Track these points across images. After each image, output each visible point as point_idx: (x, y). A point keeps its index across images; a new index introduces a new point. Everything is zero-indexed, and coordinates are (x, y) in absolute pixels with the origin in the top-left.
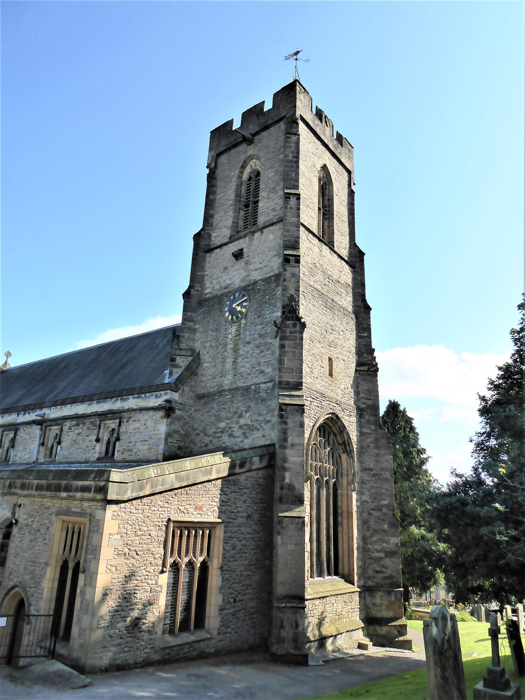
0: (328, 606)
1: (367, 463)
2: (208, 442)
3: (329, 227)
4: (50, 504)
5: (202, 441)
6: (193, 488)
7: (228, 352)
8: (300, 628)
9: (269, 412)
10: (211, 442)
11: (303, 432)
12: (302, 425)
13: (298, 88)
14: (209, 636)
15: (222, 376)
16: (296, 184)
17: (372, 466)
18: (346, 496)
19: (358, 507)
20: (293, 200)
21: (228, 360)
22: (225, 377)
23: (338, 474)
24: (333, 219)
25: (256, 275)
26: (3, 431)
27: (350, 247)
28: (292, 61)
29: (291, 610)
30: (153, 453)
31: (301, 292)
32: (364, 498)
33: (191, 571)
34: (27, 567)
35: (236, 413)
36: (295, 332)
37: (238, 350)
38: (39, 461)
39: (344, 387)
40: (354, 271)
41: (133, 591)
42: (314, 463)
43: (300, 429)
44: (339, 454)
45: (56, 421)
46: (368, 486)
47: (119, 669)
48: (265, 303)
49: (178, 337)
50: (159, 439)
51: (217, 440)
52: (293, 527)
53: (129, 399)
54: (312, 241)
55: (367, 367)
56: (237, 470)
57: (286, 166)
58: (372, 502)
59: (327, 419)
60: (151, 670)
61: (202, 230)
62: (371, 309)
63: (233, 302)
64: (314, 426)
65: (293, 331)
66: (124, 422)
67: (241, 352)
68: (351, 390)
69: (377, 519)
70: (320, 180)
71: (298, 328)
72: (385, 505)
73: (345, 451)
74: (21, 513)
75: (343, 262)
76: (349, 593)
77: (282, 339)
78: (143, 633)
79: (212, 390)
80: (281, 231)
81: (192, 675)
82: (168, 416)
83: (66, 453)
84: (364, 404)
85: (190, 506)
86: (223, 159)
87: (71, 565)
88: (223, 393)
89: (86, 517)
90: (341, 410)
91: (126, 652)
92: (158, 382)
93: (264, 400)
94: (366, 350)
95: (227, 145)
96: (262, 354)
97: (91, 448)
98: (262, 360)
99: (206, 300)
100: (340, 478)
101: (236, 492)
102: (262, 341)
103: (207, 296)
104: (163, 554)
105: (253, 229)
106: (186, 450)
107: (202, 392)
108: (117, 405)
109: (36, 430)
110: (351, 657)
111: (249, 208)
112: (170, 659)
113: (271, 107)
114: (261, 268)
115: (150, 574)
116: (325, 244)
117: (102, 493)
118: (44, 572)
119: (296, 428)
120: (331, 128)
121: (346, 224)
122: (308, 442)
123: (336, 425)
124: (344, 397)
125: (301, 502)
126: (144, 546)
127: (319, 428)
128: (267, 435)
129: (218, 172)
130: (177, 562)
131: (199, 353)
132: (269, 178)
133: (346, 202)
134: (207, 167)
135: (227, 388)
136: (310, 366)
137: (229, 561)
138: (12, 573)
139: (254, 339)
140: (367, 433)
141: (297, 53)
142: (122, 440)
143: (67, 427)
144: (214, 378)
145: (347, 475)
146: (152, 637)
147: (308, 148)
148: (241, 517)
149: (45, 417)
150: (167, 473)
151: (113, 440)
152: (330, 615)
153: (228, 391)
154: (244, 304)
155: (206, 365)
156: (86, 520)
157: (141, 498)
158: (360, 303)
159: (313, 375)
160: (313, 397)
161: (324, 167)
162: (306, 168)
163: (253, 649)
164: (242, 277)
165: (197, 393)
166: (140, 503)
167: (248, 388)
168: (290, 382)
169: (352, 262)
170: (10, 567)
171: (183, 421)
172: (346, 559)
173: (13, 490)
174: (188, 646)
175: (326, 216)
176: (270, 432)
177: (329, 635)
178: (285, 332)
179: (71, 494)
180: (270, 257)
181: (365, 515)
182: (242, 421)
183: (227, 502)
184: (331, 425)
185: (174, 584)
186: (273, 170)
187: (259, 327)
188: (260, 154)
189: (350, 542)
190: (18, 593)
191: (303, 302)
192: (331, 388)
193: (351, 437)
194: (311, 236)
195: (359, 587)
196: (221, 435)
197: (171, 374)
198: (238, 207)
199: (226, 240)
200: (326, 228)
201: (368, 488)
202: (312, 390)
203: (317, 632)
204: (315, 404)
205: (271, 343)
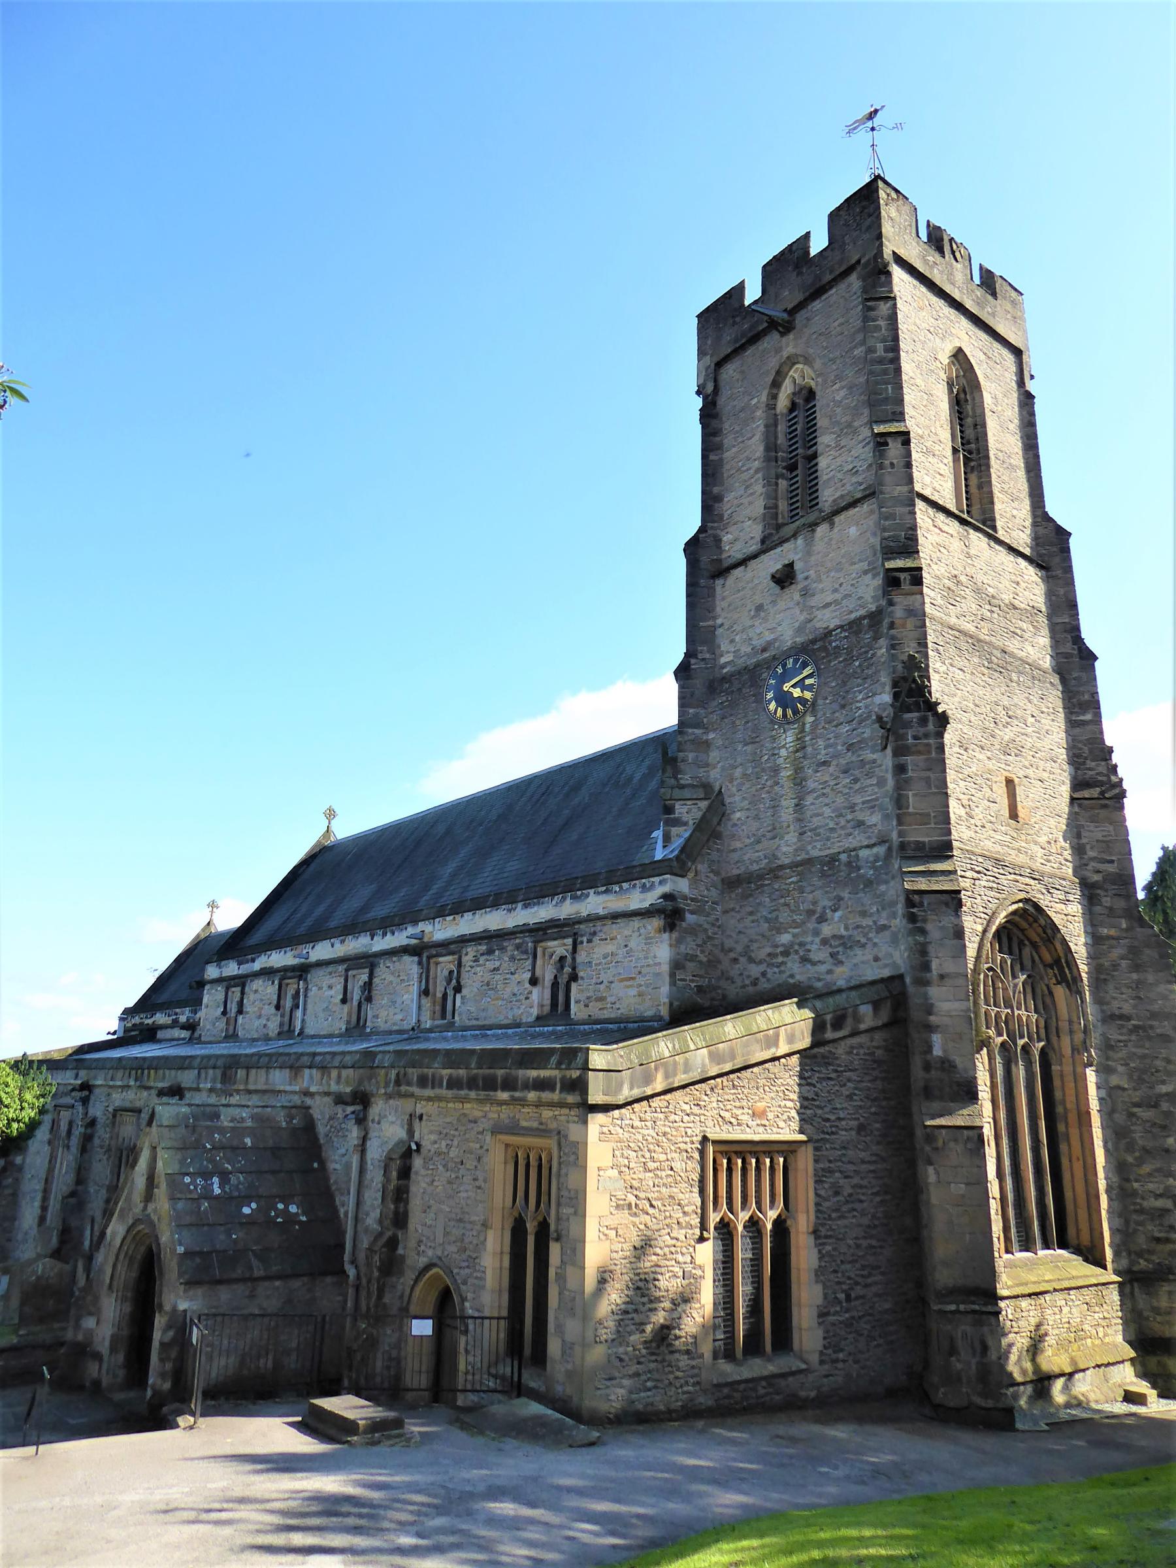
0: (1049, 1312)
1: (1115, 1004)
2: (759, 975)
3: (980, 487)
4: (478, 1114)
5: (746, 973)
6: (744, 1074)
7: (782, 786)
8: (993, 1356)
9: (883, 909)
10: (764, 974)
11: (964, 947)
12: (959, 933)
13: (882, 194)
14: (804, 1366)
15: (774, 838)
16: (899, 410)
17: (1127, 1008)
18: (1072, 1078)
19: (1101, 1099)
20: (894, 449)
21: (784, 803)
22: (782, 838)
23: (1049, 1030)
24: (988, 466)
25: (828, 616)
26: (347, 970)
27: (1035, 524)
28: (863, 136)
29: (970, 1317)
30: (648, 1003)
31: (930, 645)
32: (1115, 1080)
33: (754, 1237)
34: (448, 1230)
35: (810, 913)
36: (926, 736)
37: (804, 779)
38: (423, 1026)
39: (1045, 839)
40: (1048, 577)
41: (652, 1276)
42: (993, 1011)
43: (955, 942)
44: (1048, 986)
45: (445, 947)
46: (1122, 1054)
47: (638, 1420)
48: (854, 675)
49: (674, 760)
50: (658, 974)
51: (776, 970)
52: (959, 1148)
53: (588, 896)
54: (945, 528)
55: (1096, 787)
56: (829, 1035)
57: (871, 373)
58: (1135, 1089)
59: (1014, 913)
60: (700, 1424)
61: (702, 530)
62: (1096, 658)
63: (784, 678)
64: (985, 931)
65: (920, 734)
66: (582, 942)
67: (811, 784)
68: (1063, 844)
69: (1148, 1125)
70: (950, 385)
71: (931, 727)
72: (1167, 1094)
73: (1062, 980)
74: (425, 1131)
75: (1020, 560)
76: (1096, 1285)
77: (898, 752)
78: (677, 1355)
79: (755, 867)
80: (875, 516)
81: (778, 1436)
82: (670, 926)
83: (472, 1009)
84: (1098, 872)
85: (741, 1111)
86: (730, 371)
87: (531, 1227)
88: (780, 873)
89: (549, 1137)
90: (1044, 891)
91: (649, 1390)
92: (641, 858)
93: (869, 883)
94: (1091, 751)
95: (736, 341)
96: (857, 786)
97: (522, 997)
98: (858, 799)
99: (724, 679)
100: (1054, 1039)
101: (830, 1079)
102: (854, 759)
103: (725, 671)
104: (699, 1204)
105: (812, 517)
106: (713, 994)
107: (736, 872)
108: (565, 909)
109: (410, 965)
110: (1107, 1417)
111: (799, 471)
112: (726, 1407)
113: (825, 243)
114: (836, 602)
115: (679, 1244)
116: (977, 529)
117: (577, 1093)
118: (482, 1239)
119: (947, 941)
120: (967, 263)
121: (1021, 474)
122: (975, 965)
123: (1035, 925)
124: (1049, 861)
125: (972, 1096)
126: (664, 1190)
127: (998, 934)
128: (883, 956)
129: (721, 401)
130: (726, 1220)
131: (720, 791)
132: (836, 400)
133: (1016, 421)
134: (698, 393)
135: (787, 861)
136: (965, 802)
137: (830, 1218)
138: (421, 1241)
139: (836, 756)
140: (1109, 937)
141: (872, 115)
142: (582, 978)
143: (470, 957)
144: (759, 842)
145: (1071, 1032)
146: (694, 1363)
147: (918, 322)
148: (846, 1130)
149: (426, 940)
150: (692, 1047)
151: (563, 980)
152: (1056, 1332)
153: (791, 868)
154: (807, 682)
155: (738, 815)
156: (552, 1143)
157: (647, 1098)
158: (1068, 647)
159: (973, 821)
160: (977, 869)
161: (959, 356)
162: (918, 367)
163: (892, 1394)
164: (797, 625)
165: (724, 875)
166: (648, 1109)
167: (833, 859)
168: (923, 843)
169: (1040, 555)
170: (417, 1231)
171: (702, 936)
172: (1083, 1214)
173: (403, 1088)
174: (764, 1383)
175: (972, 464)
176: (890, 949)
177: (1057, 1370)
178: (903, 737)
179: (517, 1094)
180: (854, 575)
181: (1120, 1118)
182: (827, 930)
183: (813, 1099)
184: (1024, 925)
185: (724, 1262)
186: (843, 383)
187: (845, 728)
188: (811, 351)
189: (1090, 1177)
190: (437, 1277)
191: (936, 665)
192: (1016, 845)
193: (1073, 947)
194: (941, 517)
195: (1117, 1272)
196: (785, 959)
197: (667, 839)
198: (773, 472)
199: (754, 547)
200: (974, 490)
201: (1122, 1059)
202: (973, 853)
203: (1028, 1366)
204: (983, 883)
205: (874, 761)
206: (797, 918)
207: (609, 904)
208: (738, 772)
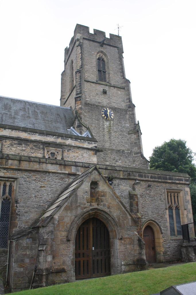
98: (123, 141)
207: (76, 144)
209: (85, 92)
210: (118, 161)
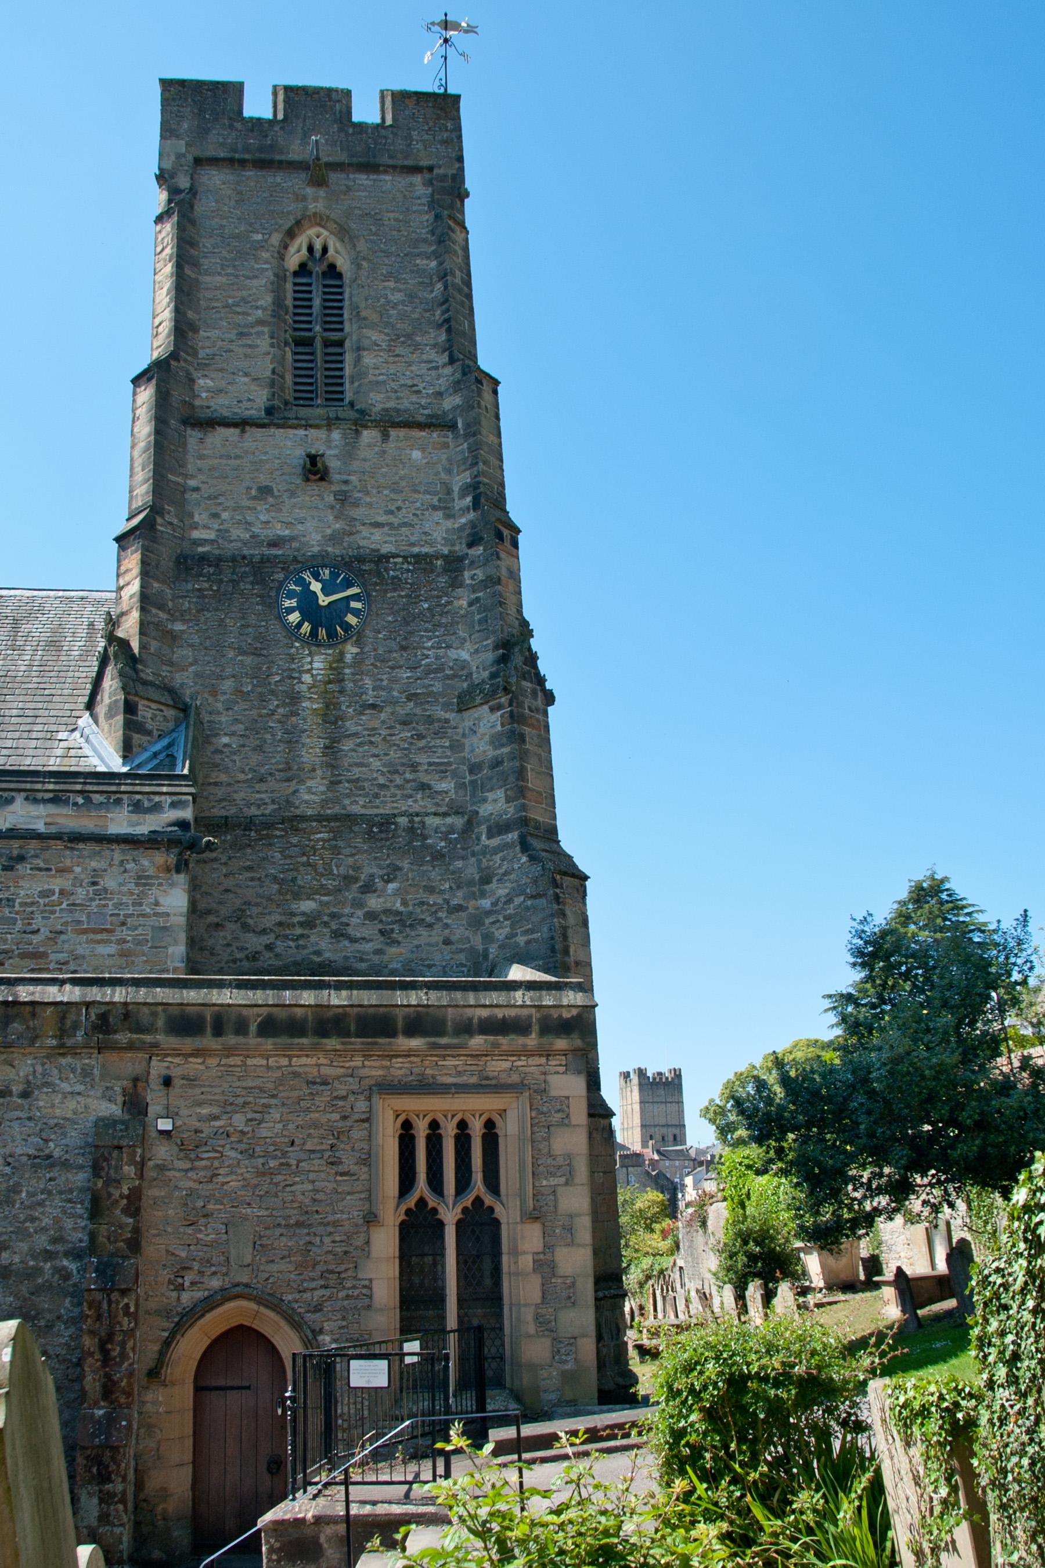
9: (458, 887)
15: (288, 780)
22: (302, 782)
35: (349, 880)
79: (254, 811)
96: (422, 743)
98: (423, 759)
118: (359, 1242)
153: (319, 821)
167: (386, 823)
180: (418, 504)
182: (374, 903)
205: (447, 721)
206: (330, 884)
207: (60, 820)
208: (228, 685)
209: (184, 489)
210: (379, 884)
